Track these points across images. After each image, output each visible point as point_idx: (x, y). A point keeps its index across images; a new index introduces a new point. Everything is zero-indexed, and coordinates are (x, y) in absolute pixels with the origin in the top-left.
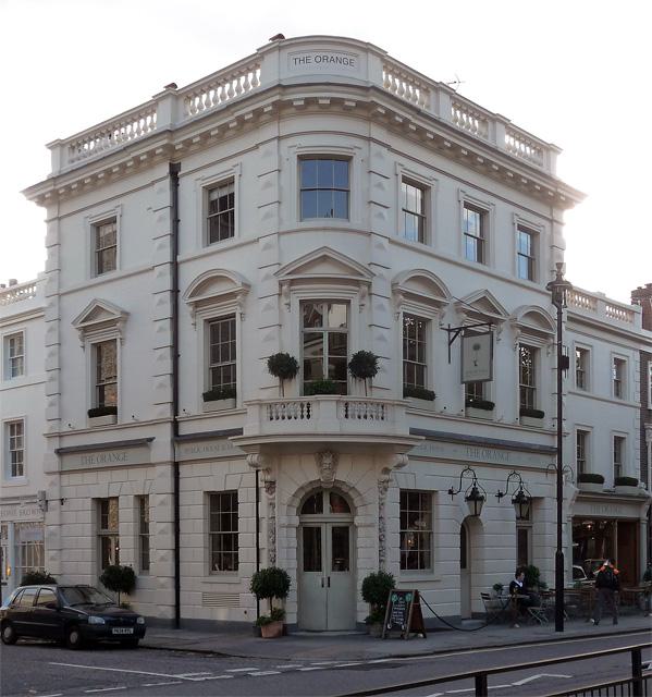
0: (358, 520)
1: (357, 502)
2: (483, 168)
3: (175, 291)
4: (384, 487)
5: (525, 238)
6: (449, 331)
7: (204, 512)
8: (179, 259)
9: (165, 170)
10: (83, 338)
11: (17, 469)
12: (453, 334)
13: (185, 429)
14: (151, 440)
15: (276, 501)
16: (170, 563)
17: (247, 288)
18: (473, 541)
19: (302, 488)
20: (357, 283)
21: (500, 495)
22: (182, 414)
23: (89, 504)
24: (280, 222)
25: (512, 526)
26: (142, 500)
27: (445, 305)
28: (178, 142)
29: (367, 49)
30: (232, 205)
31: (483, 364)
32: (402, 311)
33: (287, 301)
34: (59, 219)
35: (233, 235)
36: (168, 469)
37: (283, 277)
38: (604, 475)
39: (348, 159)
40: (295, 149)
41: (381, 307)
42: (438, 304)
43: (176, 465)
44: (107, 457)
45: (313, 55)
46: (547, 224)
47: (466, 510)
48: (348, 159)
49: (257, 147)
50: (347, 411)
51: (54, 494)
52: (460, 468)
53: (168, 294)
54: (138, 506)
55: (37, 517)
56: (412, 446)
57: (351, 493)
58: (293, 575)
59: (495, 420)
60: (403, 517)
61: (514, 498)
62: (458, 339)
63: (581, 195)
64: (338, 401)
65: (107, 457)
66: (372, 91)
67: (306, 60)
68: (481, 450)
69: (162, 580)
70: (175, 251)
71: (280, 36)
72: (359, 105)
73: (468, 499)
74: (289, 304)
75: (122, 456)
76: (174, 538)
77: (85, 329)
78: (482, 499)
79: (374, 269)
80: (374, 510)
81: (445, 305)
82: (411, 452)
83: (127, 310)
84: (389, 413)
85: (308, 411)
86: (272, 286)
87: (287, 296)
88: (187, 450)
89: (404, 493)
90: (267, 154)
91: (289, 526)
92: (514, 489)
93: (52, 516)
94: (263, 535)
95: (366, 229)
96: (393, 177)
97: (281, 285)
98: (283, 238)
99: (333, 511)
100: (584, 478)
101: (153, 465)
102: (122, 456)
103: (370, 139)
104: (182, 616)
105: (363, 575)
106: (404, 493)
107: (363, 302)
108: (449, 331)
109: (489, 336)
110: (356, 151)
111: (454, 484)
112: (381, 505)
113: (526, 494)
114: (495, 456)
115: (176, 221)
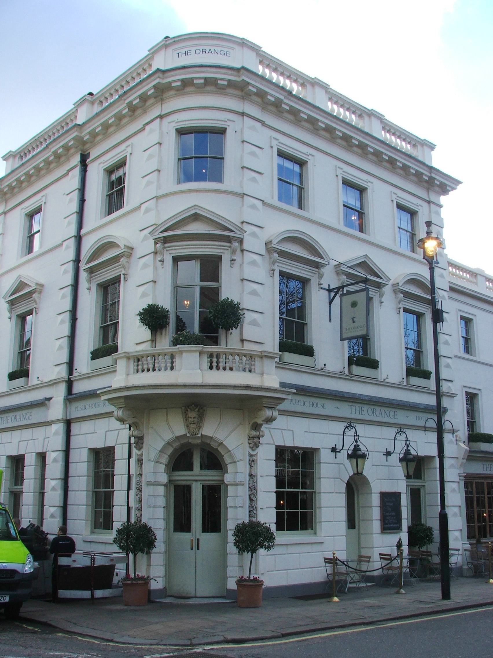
0: (228, 478)
1: (227, 459)
2: (359, 151)
3: (77, 261)
5: (405, 217)
6: (330, 291)
7: (88, 469)
8: (83, 232)
9: (76, 159)
10: (11, 310)
12: (332, 294)
13: (79, 388)
14: (49, 399)
17: (129, 251)
19: (169, 444)
20: (228, 239)
21: (388, 454)
22: (75, 374)
24: (159, 187)
26: (42, 457)
29: (243, 43)
31: (361, 320)
36: (60, 428)
37: (157, 235)
39: (222, 131)
40: (174, 124)
41: (254, 263)
43: (68, 423)
44: (18, 417)
45: (193, 49)
46: (425, 204)
48: (222, 131)
52: (343, 425)
53: (71, 264)
54: (39, 464)
56: (283, 399)
57: (219, 449)
58: (160, 535)
59: (379, 379)
62: (337, 298)
63: (458, 182)
64: (201, 353)
66: (242, 71)
67: (187, 53)
68: (366, 408)
70: (80, 226)
71: (167, 37)
72: (231, 84)
73: (350, 457)
74: (162, 261)
78: (364, 456)
82: (282, 407)
86: (149, 246)
87: (162, 254)
88: (76, 408)
92: (400, 448)
94: (132, 493)
95: (238, 190)
96: (267, 149)
97: (156, 243)
98: (161, 201)
99: (203, 467)
102: (28, 415)
103: (243, 114)
107: (234, 258)
108: (330, 291)
109: (365, 292)
110: (229, 123)
111: (336, 441)
112: (252, 462)
113: (413, 452)
115: (82, 201)
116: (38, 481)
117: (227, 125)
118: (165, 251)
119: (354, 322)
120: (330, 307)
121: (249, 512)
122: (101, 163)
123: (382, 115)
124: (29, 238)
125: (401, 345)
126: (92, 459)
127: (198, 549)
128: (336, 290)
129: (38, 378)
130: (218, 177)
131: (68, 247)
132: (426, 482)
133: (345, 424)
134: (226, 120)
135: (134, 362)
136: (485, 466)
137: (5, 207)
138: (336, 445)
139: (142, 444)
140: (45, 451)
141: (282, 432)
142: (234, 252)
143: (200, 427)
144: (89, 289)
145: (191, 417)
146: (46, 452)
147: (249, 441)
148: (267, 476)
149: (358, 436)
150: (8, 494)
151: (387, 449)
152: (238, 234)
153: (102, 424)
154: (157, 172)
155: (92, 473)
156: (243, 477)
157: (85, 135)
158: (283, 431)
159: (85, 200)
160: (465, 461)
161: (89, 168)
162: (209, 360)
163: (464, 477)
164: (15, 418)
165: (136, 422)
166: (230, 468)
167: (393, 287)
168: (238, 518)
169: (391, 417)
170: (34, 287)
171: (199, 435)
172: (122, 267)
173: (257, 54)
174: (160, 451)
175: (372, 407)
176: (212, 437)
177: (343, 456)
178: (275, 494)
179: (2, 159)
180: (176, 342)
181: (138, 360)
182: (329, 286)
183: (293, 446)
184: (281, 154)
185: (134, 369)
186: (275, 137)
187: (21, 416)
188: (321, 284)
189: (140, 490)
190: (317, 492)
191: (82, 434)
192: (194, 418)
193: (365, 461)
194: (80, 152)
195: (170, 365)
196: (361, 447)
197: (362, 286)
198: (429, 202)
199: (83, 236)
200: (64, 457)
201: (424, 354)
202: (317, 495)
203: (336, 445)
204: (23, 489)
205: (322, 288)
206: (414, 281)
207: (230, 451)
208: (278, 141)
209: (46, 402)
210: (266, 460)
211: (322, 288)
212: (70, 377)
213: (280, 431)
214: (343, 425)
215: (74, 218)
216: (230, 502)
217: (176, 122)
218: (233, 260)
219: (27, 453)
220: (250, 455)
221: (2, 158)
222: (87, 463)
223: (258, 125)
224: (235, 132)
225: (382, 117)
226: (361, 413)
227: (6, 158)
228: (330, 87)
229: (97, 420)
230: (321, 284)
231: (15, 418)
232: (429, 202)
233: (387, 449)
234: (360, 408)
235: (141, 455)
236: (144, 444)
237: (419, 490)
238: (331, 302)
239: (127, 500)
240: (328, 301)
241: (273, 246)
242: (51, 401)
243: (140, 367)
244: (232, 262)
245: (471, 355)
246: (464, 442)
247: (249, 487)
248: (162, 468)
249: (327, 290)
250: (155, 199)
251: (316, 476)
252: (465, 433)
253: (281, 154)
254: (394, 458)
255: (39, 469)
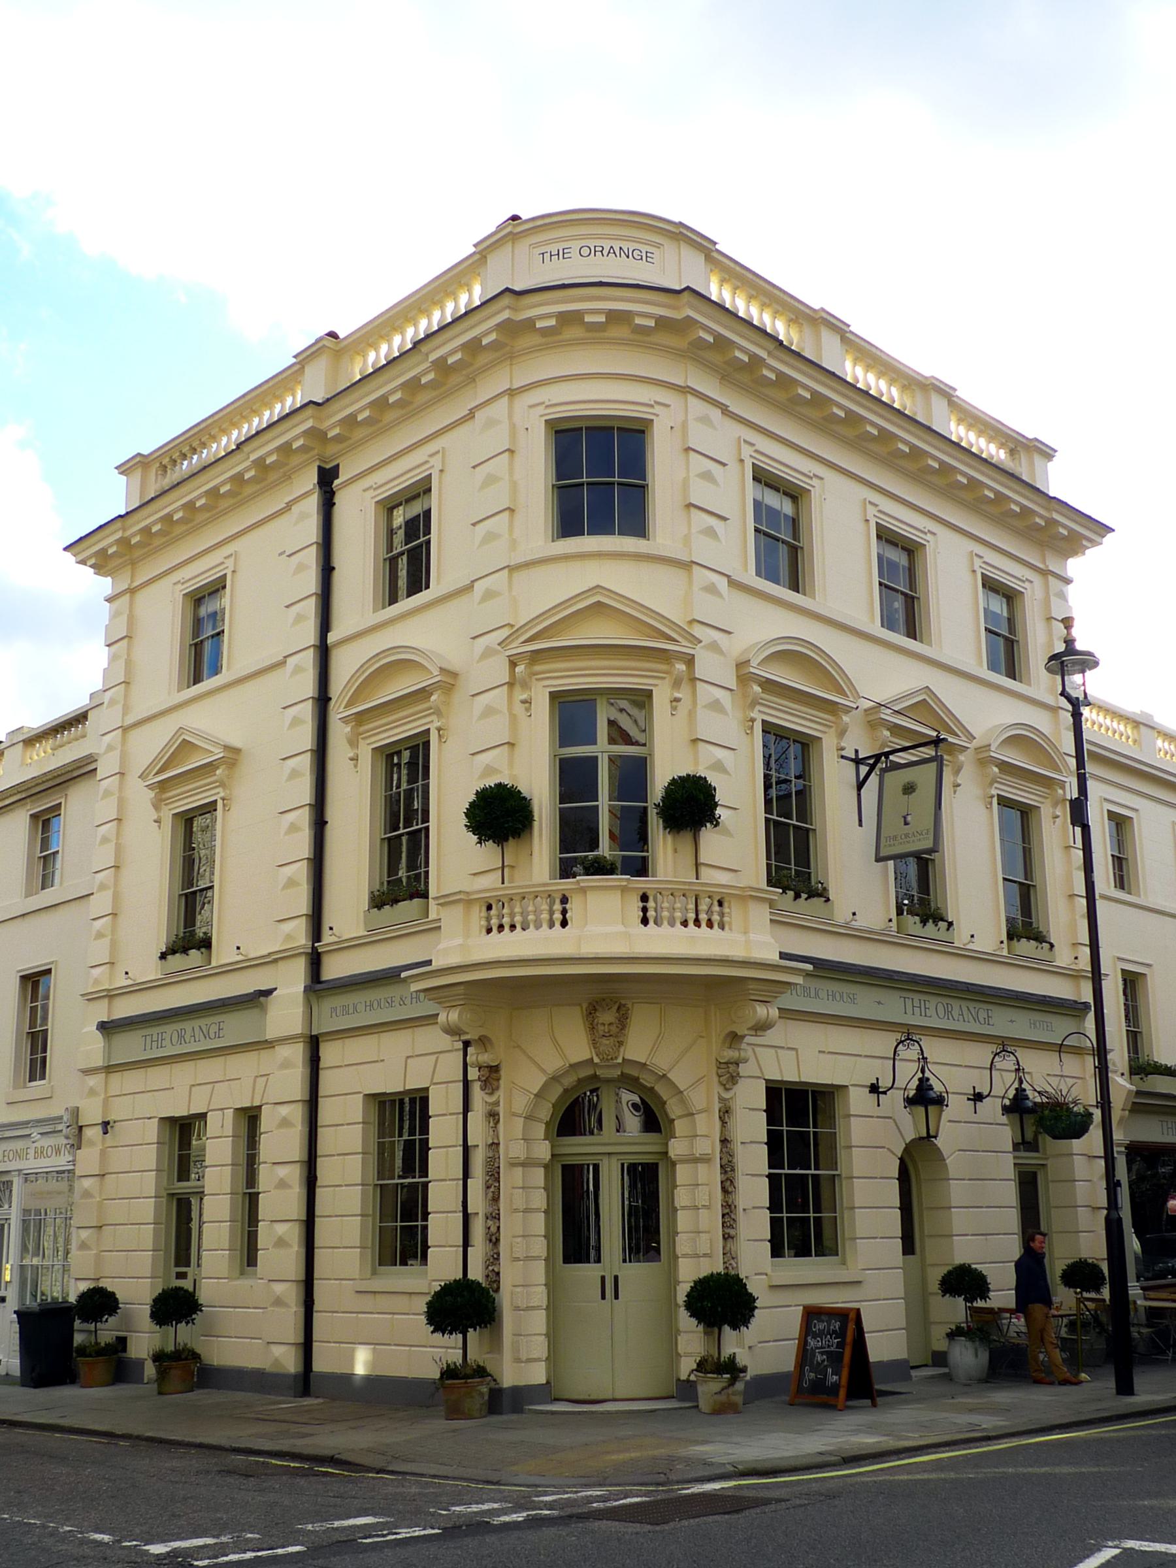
0: (676, 1148)
1: (673, 1109)
3: (323, 700)
4: (729, 1073)
6: (858, 761)
8: (332, 638)
9: (311, 478)
11: (37, 1068)
12: (864, 770)
13: (334, 969)
15: (501, 1110)
16: (296, 1249)
18: (923, 1196)
19: (555, 1079)
21: (978, 1097)
22: (327, 938)
23: (152, 1131)
25: (1006, 1166)
26: (250, 1118)
27: (848, 710)
28: (331, 423)
30: (428, 531)
32: (759, 718)
33: (524, 696)
34: (132, 591)
35: (427, 587)
36: (297, 1053)
37: (516, 648)
38: (754, 1322)
40: (541, 410)
41: (716, 706)
42: (831, 707)
43: (314, 1044)
44: (189, 1032)
47: (910, 1125)
49: (471, 415)
50: (645, 910)
51: (92, 1113)
52: (891, 1039)
54: (244, 1131)
55: (61, 1161)
60: (774, 1142)
61: (1007, 1102)
62: (874, 779)
65: (189, 1032)
67: (562, 254)
68: (932, 1002)
69: (279, 1288)
70: (325, 625)
73: (910, 1102)
75: (214, 1028)
76: (304, 1192)
77: (163, 786)
78: (940, 1101)
79: (698, 631)
80: (708, 1126)
81: (848, 710)
83: (237, 743)
84: (734, 912)
85: (564, 912)
89: (774, 1091)
90: (491, 423)
91: (527, 1164)
92: (1004, 1085)
93: (88, 1160)
94: (476, 1185)
96: (733, 466)
97: (513, 664)
98: (521, 576)
100: (1141, 1068)
101: (268, 1044)
102: (214, 1028)
104: (319, 1366)
105: (689, 1273)
106: (774, 1091)
108: (858, 761)
110: (657, 409)
112: (725, 1113)
114: (962, 1016)
115: (327, 570)
116: (242, 1171)
117: (654, 414)
118: (533, 680)
119: (906, 823)
120: (859, 795)
121: (723, 1216)
122: (371, 487)
123: (951, 388)
124: (193, 648)
125: (996, 876)
126: (374, 1118)
127: (617, 1297)
128: (871, 761)
129: (238, 948)
130: (637, 525)
131: (298, 669)
132: (1046, 1159)
133: (898, 1036)
134: (652, 403)
135: (480, 911)
136: (1165, 1124)
137: (132, 582)
138: (877, 1079)
139: (498, 1080)
140: (257, 1104)
141: (776, 1052)
142: (677, 684)
143: (621, 1043)
144: (355, 759)
145: (604, 1025)
146: (260, 1107)
147: (720, 1071)
148: (751, 1142)
149: (925, 1059)
150: (164, 1200)
151: (974, 1088)
152: (684, 647)
153: (395, 1045)
154: (507, 513)
155: (373, 1148)
156: (709, 1145)
157: (333, 426)
158: (779, 1051)
159: (334, 568)
160: (1127, 1112)
161: (337, 499)
162: (641, 905)
163: (1126, 1148)
164: (181, 1037)
165: (485, 1037)
166: (680, 1127)
167: (977, 753)
168: (701, 1230)
169: (982, 1021)
170: (218, 753)
171: (620, 1060)
172: (433, 713)
173: (706, 259)
174: (535, 1095)
175: (946, 1001)
176: (645, 1064)
177: (894, 1101)
178: (767, 1180)
179: (116, 471)
180: (566, 870)
181: (489, 908)
182: (857, 751)
183: (798, 1080)
184: (761, 477)
185: (481, 926)
186: (748, 440)
187: (197, 1030)
188: (843, 749)
189: (493, 1175)
190: (844, 1176)
191: (417, 1056)
192: (610, 1024)
193: (942, 1111)
194: (317, 463)
195: (561, 917)
196: (933, 1082)
197: (929, 752)
198: (1045, 573)
199: (335, 645)
200: (307, 1116)
201: (835, 906)
202: (844, 1183)
203: (877, 1079)
204: (203, 1187)
205: (843, 757)
206: (1020, 740)
207: (682, 1092)
208: (754, 448)
209: (262, 999)
210: (750, 1109)
211: (843, 757)
212: (316, 945)
213: (772, 1051)
214: (891, 1039)
215: (311, 607)
216: (682, 1197)
217: (547, 406)
218: (677, 700)
219: (267, 1104)
220: (721, 1099)
221: (116, 468)
222: (361, 1125)
223: (716, 414)
224: (672, 428)
225: (951, 392)
226: (923, 1014)
227: (125, 469)
228: (851, 328)
229: (347, 1040)
230: (843, 749)
231: (181, 1037)
232: (1045, 573)
233: (974, 1088)
234: (922, 1002)
235: (497, 1103)
236: (501, 1082)
237: (1035, 1174)
238: (860, 785)
239: (461, 1199)
240: (855, 784)
241: (752, 670)
242: (270, 997)
243: (494, 922)
244: (674, 704)
245: (1130, 893)
246: (1123, 1074)
247: (721, 1166)
248: (540, 1130)
249: (852, 760)
250: (506, 571)
251: (841, 1141)
252: (1123, 1057)
253: (761, 477)
254: (992, 1108)
255: (243, 1143)
